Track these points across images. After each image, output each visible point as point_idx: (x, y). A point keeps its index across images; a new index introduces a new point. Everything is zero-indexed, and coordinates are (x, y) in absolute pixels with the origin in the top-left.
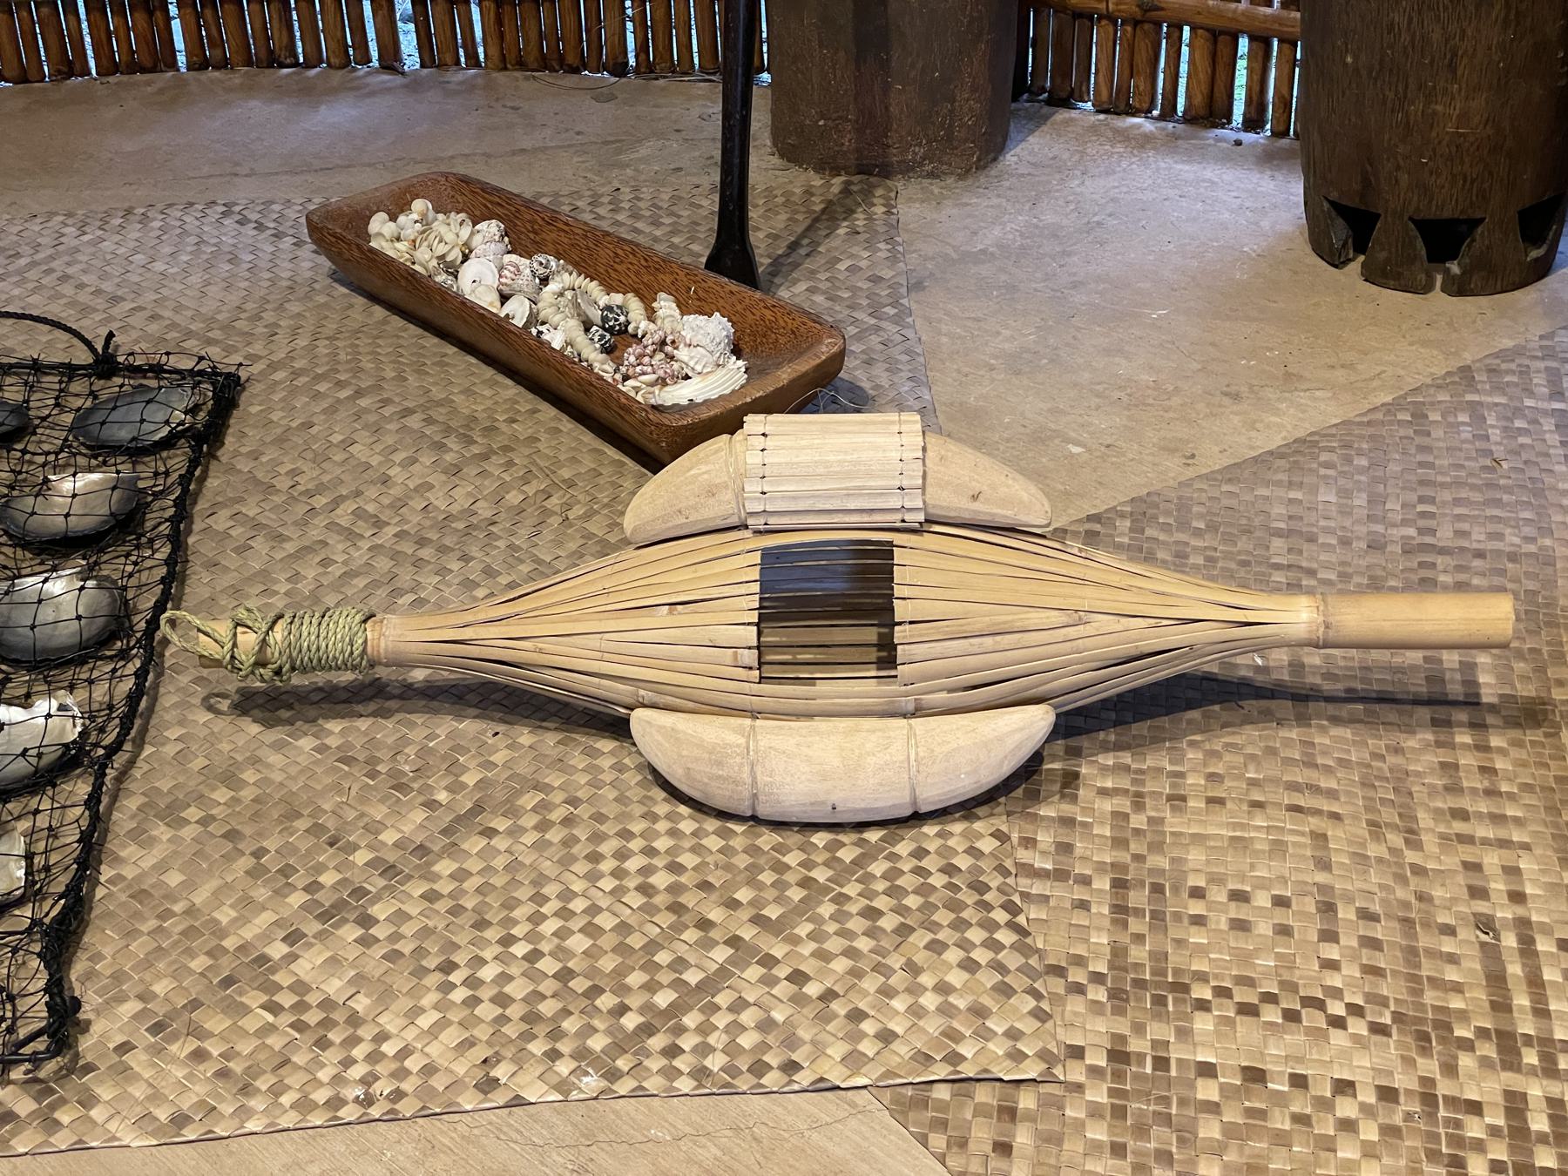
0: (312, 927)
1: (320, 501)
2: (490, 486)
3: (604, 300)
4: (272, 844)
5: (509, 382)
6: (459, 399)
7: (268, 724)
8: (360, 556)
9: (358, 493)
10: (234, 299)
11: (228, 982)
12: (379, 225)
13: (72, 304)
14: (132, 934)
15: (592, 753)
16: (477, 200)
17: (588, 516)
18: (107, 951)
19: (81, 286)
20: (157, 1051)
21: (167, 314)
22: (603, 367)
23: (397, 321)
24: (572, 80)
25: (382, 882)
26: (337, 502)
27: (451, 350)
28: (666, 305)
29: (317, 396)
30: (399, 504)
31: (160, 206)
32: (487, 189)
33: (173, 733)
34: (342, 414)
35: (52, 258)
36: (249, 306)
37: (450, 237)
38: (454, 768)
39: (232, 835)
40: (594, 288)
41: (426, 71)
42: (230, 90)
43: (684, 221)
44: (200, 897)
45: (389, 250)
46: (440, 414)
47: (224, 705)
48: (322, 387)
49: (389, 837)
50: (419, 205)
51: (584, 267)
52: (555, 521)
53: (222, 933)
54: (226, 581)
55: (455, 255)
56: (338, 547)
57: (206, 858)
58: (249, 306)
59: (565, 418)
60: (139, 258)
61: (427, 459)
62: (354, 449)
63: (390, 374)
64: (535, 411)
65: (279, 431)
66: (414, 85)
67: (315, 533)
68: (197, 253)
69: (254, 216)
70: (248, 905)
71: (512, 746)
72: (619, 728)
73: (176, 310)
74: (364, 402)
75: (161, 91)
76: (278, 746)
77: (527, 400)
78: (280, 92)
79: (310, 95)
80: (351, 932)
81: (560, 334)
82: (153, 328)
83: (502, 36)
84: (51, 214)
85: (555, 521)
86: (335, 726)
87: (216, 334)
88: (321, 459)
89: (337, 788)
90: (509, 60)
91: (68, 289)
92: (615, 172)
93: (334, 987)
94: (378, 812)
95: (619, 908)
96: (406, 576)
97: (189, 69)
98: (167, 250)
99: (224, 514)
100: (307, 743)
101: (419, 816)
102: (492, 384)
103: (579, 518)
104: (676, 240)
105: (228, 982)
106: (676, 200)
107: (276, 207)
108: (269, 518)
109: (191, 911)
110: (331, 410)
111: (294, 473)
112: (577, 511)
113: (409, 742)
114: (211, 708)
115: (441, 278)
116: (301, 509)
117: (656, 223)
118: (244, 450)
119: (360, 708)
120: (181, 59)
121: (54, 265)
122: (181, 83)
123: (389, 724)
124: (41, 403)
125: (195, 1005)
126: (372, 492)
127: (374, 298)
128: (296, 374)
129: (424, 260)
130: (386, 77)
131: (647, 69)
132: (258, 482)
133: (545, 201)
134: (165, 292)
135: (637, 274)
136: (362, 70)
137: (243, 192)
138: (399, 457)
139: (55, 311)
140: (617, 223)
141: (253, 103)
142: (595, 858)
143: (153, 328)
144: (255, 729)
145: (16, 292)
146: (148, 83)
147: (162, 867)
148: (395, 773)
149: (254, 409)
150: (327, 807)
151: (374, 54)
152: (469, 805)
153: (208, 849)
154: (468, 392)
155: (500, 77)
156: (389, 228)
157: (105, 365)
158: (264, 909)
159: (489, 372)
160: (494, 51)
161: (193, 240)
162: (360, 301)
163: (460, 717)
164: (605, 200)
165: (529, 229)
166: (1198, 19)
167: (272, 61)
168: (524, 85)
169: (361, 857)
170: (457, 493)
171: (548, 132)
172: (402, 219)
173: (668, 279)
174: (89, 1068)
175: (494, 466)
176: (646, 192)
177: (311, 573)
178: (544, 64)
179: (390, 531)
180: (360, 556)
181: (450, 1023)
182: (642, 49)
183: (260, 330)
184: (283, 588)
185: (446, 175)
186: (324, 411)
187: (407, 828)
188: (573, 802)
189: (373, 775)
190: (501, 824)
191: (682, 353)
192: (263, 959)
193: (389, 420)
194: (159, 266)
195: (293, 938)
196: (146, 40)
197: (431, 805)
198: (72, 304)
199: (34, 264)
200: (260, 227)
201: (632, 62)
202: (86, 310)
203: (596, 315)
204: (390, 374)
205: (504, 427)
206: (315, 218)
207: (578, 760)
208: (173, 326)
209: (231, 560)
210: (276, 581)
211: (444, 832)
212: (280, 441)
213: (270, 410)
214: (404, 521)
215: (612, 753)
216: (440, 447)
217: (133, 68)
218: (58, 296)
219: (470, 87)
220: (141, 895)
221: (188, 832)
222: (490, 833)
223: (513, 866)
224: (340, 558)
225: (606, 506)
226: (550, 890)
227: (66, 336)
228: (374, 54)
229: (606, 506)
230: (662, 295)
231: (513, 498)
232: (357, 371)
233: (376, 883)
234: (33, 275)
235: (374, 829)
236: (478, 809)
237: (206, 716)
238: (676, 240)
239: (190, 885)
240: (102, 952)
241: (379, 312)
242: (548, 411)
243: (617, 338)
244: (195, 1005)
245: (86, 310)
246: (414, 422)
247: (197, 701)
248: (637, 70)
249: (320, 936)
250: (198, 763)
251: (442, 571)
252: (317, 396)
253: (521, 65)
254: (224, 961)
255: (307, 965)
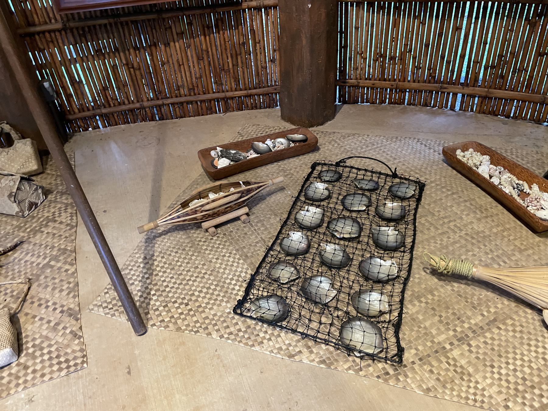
0: (456, 343)
1: (446, 220)
2: (488, 226)
3: (517, 182)
4: (444, 314)
5: (489, 197)
6: (477, 199)
7: (440, 280)
8: (457, 237)
9: (455, 221)
10: (421, 163)
11: (436, 352)
12: (459, 152)
13: (386, 158)
14: (412, 330)
15: (526, 313)
16: (483, 150)
17: (515, 239)
18: (407, 333)
19: (387, 154)
20: (421, 366)
21: (406, 164)
22: (518, 200)
23: (459, 175)
24: (495, 118)
25: (472, 335)
26: (450, 222)
27: (474, 185)
28: (535, 187)
29: (443, 192)
30: (465, 226)
31: (404, 137)
32: (486, 147)
33: (417, 276)
34: (450, 198)
35: (381, 146)
36: (424, 165)
37: (477, 159)
38: (488, 307)
39: (433, 309)
40: (515, 178)
41: (461, 111)
42: (416, 111)
43: (530, 160)
44: (427, 324)
45: (460, 158)
46: (473, 203)
47: (428, 271)
48: (444, 190)
49: (473, 322)
50: (471, 150)
51: (510, 172)
52: (506, 239)
53: (433, 337)
54: (426, 237)
55: (479, 163)
56: (451, 235)
57: (428, 313)
58: (424, 165)
59: (505, 210)
60: (399, 149)
61: (472, 215)
62: (454, 208)
63: (460, 189)
64: (497, 206)
65: (434, 199)
66: (458, 115)
67: (445, 229)
68: (412, 150)
69: (424, 143)
70: (440, 333)
71: (503, 303)
72: (540, 311)
73: (408, 164)
74: (455, 196)
75: (402, 109)
76: (442, 286)
77: (495, 203)
78: (428, 113)
79: (434, 114)
80: (466, 348)
81: (508, 190)
82: (404, 167)
83: (481, 106)
84: (381, 136)
85: (506, 239)
86: (456, 285)
87: (417, 171)
88: (445, 209)
89: (458, 303)
90: (481, 111)
91: (385, 155)
92: (510, 144)
93: (463, 362)
94: (469, 313)
95: (529, 355)
96: (469, 246)
97: (407, 105)
98: (406, 148)
99: (423, 219)
100: (449, 288)
101: (480, 318)
102: (485, 197)
103: (513, 240)
104: (528, 165)
105: (436, 352)
106: (527, 154)
107: (429, 141)
108: (434, 222)
109: (425, 328)
110: (447, 197)
111: (439, 211)
112: (511, 238)
113: (475, 295)
114: (425, 271)
115: (474, 168)
116: (441, 222)
117: (523, 160)
118: (427, 203)
119: (461, 281)
120: (406, 103)
121: (382, 148)
122: (406, 108)
123: (469, 288)
124: (381, 182)
125: (429, 356)
126: (458, 221)
127: (454, 168)
128: (437, 185)
129: (470, 163)
130: (451, 112)
131: (515, 118)
132: (430, 212)
133: (494, 149)
134: (406, 159)
135: (527, 177)
136: (446, 110)
137: (421, 136)
138: (465, 213)
139: (384, 161)
140: (512, 158)
141: (422, 115)
142: (529, 345)
143: (404, 167)
144: (436, 280)
145: (374, 153)
146: (399, 107)
147: (417, 313)
148: (472, 303)
149: (428, 192)
150: (456, 308)
151: (449, 106)
152: (493, 318)
153: (428, 311)
154: (479, 198)
155: (479, 115)
156: (462, 154)
157: (395, 175)
158: (443, 333)
159: (484, 193)
160: (478, 109)
161: (411, 147)
162: (450, 168)
163: (488, 291)
164: (509, 151)
165: (497, 159)
166: (518, 98)
167: (426, 105)
168: (485, 118)
169: (466, 325)
170: (480, 226)
171: (492, 131)
172: (466, 153)
173: (537, 180)
174: (405, 366)
175: (489, 220)
176: (519, 151)
177: (445, 240)
178: (490, 113)
179: (464, 232)
180: (457, 237)
181: (494, 384)
182: (515, 113)
183: (428, 172)
184: (439, 242)
185: (475, 142)
186: (445, 197)
187: (477, 320)
188: (522, 326)
189: (467, 302)
190: (503, 327)
191: (542, 202)
192: (444, 348)
193: (461, 202)
194: (404, 152)
195: (451, 344)
196: (400, 98)
197: (483, 315)
198: (386, 158)
199: (377, 147)
200: (425, 146)
201: (512, 115)
202: (389, 160)
203: (515, 186)
204: (460, 189)
205: (489, 209)
206: (445, 149)
207: (521, 313)
208: (408, 167)
209: (426, 232)
210: (437, 240)
211: (487, 324)
212: (435, 202)
213: (431, 193)
214: (467, 231)
215: (531, 313)
216: (475, 212)
217: (395, 103)
218: (382, 156)
219: (471, 117)
220: (413, 320)
221: (423, 305)
222: (499, 328)
223: (507, 341)
224: (452, 237)
225: (519, 238)
226: (518, 351)
227: (385, 166)
228: (449, 106)
229: (519, 238)
230: (535, 184)
231: (495, 230)
232: (452, 187)
233: (471, 335)
234: (377, 150)
235: (469, 318)
236: (495, 320)
237: (424, 273)
238: (528, 165)
239: (424, 320)
240: (405, 332)
241: (455, 172)
242: (500, 207)
243: (523, 194)
244: (429, 356)
245: (389, 160)
246: (468, 204)
247: (421, 268)
248: (512, 118)
249: (458, 345)
250: (423, 286)
251: (479, 248)
252: (443, 192)
253: (484, 113)
254: (435, 345)
255: (456, 353)
